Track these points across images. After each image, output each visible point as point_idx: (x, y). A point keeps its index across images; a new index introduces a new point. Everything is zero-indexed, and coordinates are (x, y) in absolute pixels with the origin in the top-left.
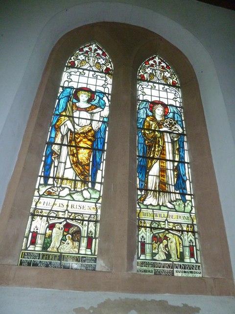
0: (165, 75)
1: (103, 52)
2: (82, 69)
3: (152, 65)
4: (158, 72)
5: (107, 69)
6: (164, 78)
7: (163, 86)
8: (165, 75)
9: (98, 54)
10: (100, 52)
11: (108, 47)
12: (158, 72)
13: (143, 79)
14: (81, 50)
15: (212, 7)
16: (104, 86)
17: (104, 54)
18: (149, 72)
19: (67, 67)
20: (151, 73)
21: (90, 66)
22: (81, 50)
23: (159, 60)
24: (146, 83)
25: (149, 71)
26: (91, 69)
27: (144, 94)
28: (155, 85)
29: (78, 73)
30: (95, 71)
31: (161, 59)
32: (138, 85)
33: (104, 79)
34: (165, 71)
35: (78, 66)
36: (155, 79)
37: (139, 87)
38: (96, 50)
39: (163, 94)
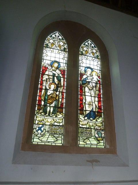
0: (60, 44)
1: (62, 38)
2: (52, 48)
3: (54, 38)
4: (56, 42)
5: (65, 49)
6: (60, 46)
7: (58, 51)
8: (60, 44)
9: (92, 47)
10: (60, 37)
11: (66, 36)
12: (56, 42)
13: (47, 46)
14: (51, 36)
15: (100, 4)
16: (64, 59)
17: (62, 39)
18: (51, 42)
19: (45, 47)
20: (52, 43)
21: (56, 47)
22: (51, 36)
23: (91, 42)
24: (49, 49)
25: (51, 41)
26: (57, 49)
27: (47, 56)
28: (54, 50)
29: (51, 51)
30: (59, 50)
31: (59, 34)
32: (44, 50)
33: (64, 54)
34: (61, 42)
35: (50, 46)
36: (88, 54)
37: (80, 58)
38: (58, 36)
39: (92, 63)
